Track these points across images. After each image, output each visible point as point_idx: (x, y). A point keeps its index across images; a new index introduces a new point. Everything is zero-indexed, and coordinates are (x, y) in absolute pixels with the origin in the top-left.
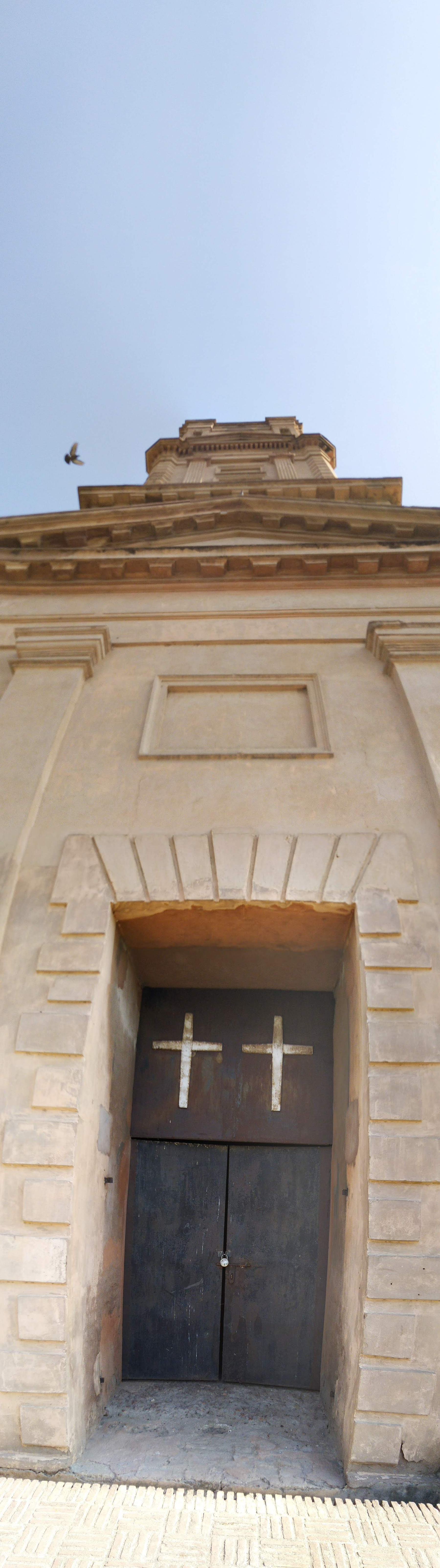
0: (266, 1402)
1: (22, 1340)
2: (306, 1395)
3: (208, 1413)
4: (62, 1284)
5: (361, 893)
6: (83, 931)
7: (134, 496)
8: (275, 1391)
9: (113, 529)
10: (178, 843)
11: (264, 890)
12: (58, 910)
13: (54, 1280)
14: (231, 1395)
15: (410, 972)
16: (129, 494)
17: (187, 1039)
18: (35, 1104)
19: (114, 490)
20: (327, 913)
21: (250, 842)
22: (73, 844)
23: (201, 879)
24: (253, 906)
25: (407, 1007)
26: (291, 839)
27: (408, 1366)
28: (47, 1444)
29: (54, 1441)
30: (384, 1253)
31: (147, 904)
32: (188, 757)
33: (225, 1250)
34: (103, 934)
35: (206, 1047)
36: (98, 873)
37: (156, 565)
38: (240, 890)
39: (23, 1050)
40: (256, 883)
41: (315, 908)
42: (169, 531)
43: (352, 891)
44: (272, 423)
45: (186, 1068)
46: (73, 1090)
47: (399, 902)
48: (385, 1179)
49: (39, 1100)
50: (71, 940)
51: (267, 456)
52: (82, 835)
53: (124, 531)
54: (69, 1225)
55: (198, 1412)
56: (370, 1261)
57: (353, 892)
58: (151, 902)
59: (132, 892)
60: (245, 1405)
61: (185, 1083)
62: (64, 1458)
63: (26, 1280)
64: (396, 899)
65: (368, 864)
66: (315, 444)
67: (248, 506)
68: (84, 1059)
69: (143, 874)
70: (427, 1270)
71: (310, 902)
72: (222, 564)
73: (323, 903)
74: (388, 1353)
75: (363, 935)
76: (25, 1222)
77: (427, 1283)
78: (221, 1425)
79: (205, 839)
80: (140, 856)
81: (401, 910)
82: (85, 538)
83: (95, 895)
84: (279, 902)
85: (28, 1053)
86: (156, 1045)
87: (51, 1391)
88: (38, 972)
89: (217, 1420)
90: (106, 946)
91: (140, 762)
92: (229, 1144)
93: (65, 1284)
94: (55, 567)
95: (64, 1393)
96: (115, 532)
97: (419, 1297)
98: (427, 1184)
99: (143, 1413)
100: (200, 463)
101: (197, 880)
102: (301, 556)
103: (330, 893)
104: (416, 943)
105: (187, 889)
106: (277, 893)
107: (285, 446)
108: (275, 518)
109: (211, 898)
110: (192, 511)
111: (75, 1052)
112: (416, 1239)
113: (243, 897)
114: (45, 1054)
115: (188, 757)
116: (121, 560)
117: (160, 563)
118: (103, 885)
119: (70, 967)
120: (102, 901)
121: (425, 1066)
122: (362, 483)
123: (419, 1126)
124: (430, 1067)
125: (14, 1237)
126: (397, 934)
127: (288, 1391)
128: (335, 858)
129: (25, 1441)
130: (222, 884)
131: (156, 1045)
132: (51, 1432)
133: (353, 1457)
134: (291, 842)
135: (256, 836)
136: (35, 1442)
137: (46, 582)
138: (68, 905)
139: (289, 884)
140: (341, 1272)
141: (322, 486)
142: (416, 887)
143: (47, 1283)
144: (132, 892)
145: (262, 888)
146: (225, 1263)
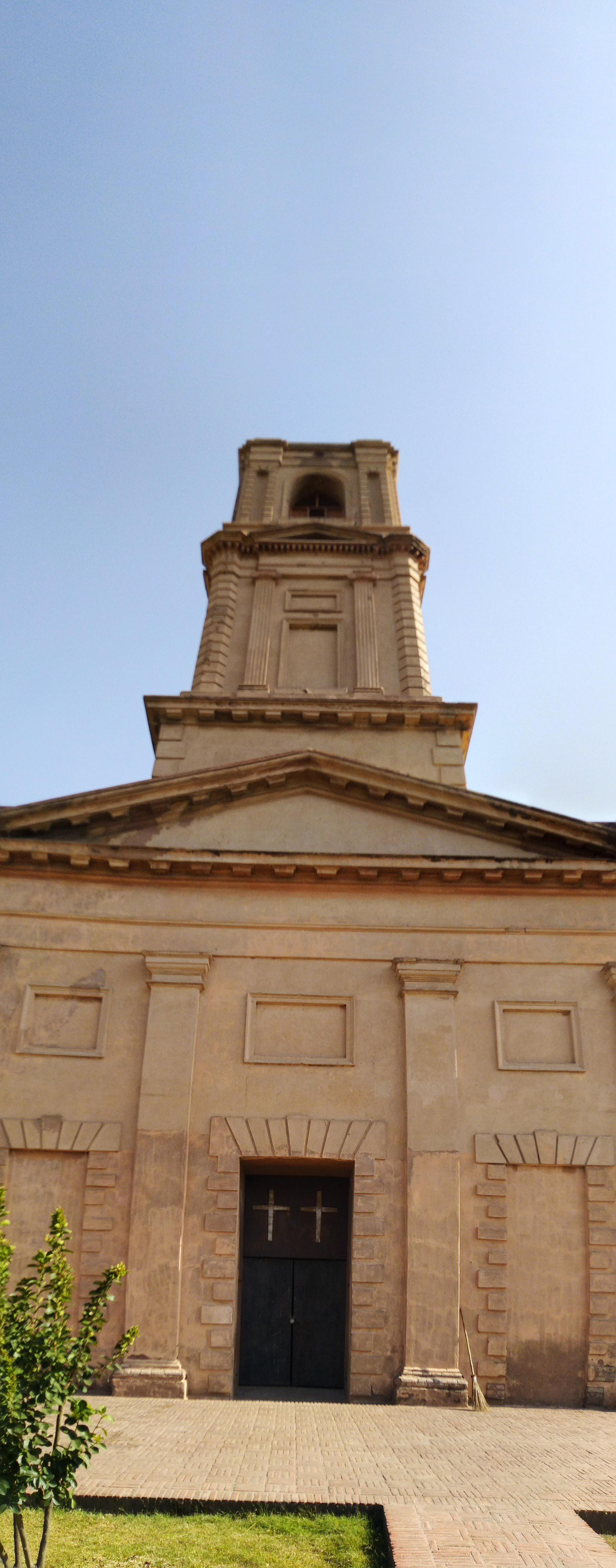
5: (358, 1155)
10: (270, 1124)
11: (313, 1152)
12: (214, 1159)
15: (375, 1196)
16: (197, 710)
17: (271, 1204)
18: (216, 1253)
21: (306, 1124)
22: (216, 1122)
26: (327, 1122)
27: (371, 1354)
33: (292, 1315)
35: (281, 1208)
36: (231, 1141)
45: (271, 1220)
46: (233, 1247)
49: (218, 1251)
50: (222, 1175)
57: (355, 1154)
59: (250, 1152)
61: (270, 1228)
72: (291, 871)
74: (362, 1349)
79: (284, 1122)
80: (252, 1131)
81: (376, 1163)
83: (231, 1153)
85: (211, 1232)
86: (255, 1208)
92: (294, 1259)
98: (376, 1283)
103: (343, 1155)
109: (287, 1156)
110: (265, 771)
114: (219, 1232)
118: (235, 1147)
120: (235, 1155)
126: (373, 1176)
129: (210, 1390)
130: (292, 1148)
131: (255, 1208)
132: (223, 1386)
133: (351, 1393)
144: (250, 1152)
146: (292, 1321)
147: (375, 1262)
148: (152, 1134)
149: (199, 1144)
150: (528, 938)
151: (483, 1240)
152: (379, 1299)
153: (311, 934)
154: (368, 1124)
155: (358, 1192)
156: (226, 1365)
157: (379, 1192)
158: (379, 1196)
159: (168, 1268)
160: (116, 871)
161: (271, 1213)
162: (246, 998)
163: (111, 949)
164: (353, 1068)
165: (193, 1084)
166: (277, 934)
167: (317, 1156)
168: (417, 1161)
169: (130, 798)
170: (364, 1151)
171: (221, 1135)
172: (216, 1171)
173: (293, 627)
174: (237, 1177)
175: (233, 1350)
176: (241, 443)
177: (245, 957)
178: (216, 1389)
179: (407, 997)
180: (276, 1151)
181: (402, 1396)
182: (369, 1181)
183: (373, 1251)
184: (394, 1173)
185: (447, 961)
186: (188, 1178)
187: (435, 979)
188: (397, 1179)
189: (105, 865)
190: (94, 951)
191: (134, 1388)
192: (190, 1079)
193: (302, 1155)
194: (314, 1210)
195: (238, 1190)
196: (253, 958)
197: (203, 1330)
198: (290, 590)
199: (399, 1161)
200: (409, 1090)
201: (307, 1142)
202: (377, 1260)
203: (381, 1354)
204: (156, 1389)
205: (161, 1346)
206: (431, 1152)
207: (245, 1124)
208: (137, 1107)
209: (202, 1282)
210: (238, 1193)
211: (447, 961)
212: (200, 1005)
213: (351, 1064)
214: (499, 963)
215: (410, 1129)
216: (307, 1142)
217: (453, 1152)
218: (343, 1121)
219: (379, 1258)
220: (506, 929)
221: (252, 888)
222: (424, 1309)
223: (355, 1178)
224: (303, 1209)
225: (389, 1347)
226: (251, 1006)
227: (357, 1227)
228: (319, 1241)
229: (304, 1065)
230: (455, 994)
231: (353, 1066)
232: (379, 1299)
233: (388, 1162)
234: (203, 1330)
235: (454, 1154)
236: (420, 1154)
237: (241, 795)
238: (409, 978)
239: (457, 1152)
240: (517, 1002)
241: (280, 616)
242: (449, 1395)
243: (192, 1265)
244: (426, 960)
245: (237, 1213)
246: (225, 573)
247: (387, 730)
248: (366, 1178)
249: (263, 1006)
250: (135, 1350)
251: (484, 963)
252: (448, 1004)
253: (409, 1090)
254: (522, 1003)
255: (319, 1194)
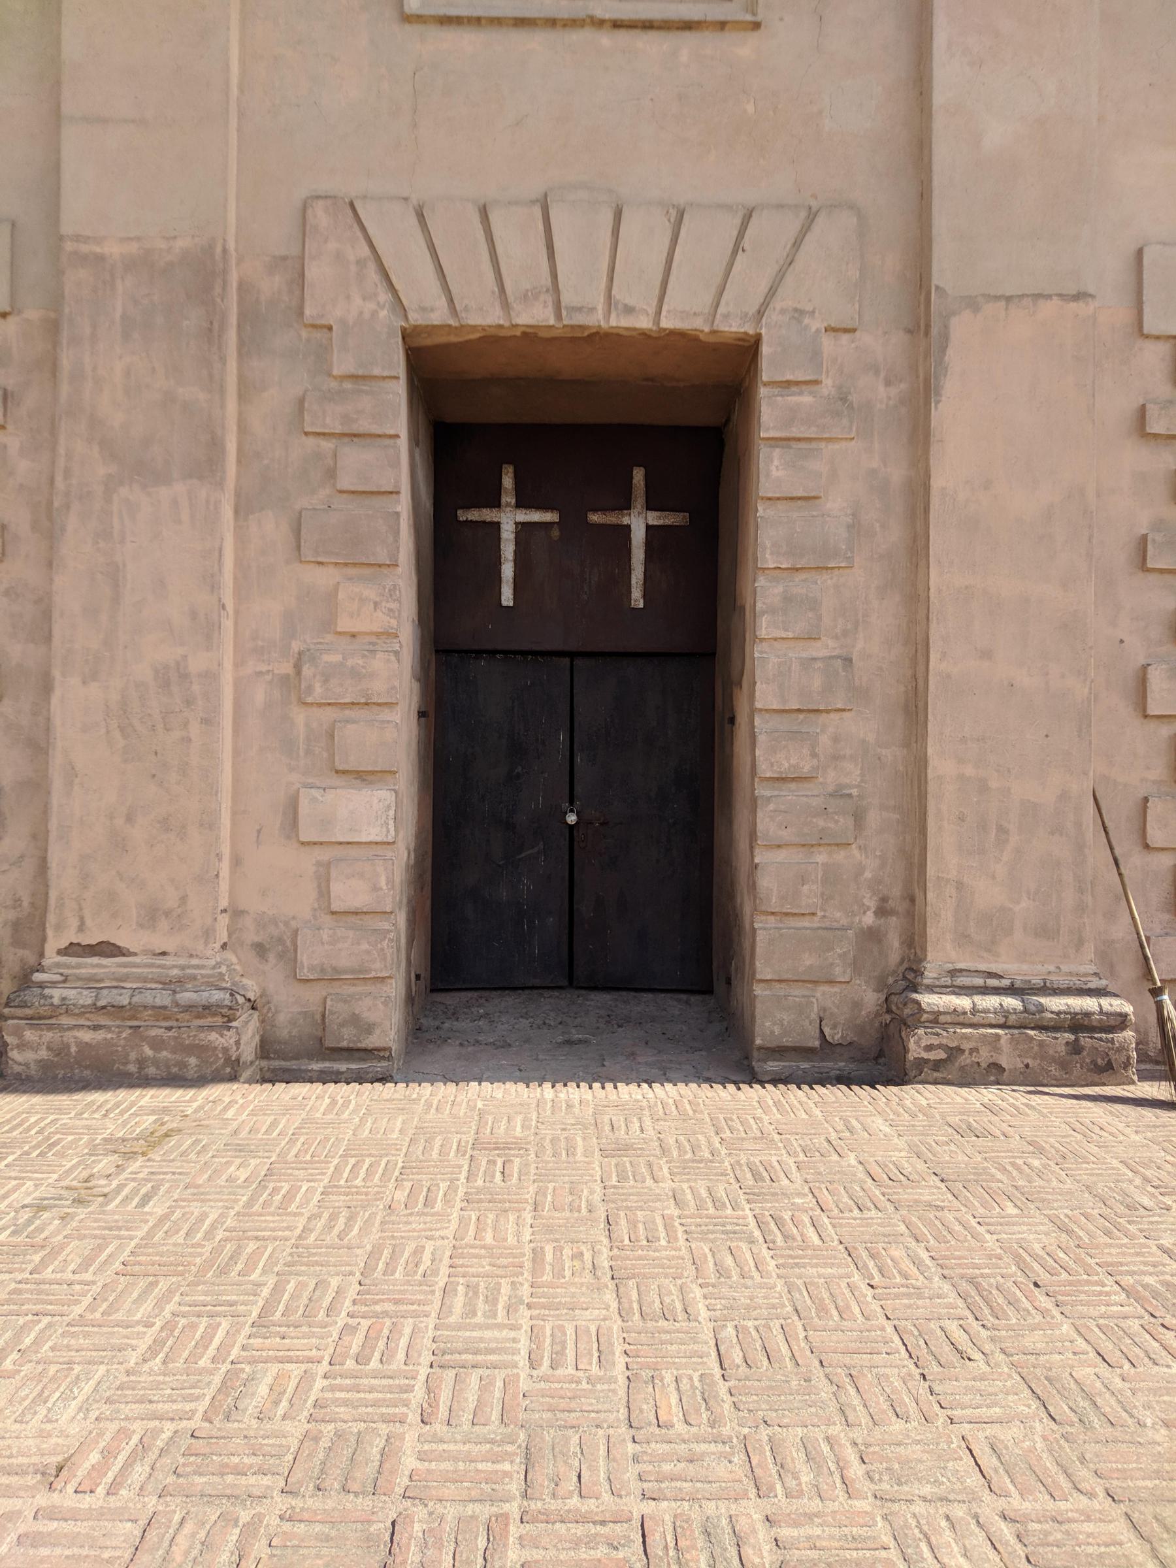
0: (639, 1009)
1: (333, 913)
2: (694, 999)
3: (561, 1023)
4: (388, 843)
5: (772, 316)
6: (366, 373)
8: (650, 996)
10: (495, 217)
11: (629, 310)
12: (318, 335)
13: (379, 839)
14: (588, 1003)
15: (823, 445)
17: (508, 505)
18: (339, 629)
21: (607, 217)
22: (320, 215)
23: (535, 288)
24: (612, 334)
25: (812, 494)
26: (673, 213)
27: (815, 923)
28: (362, 1045)
29: (373, 1041)
30: (776, 793)
32: (497, 22)
33: (571, 802)
35: (536, 516)
36: (373, 275)
38: (592, 310)
39: (313, 560)
40: (618, 297)
41: (702, 337)
45: (508, 550)
46: (391, 610)
48: (774, 707)
50: (348, 385)
52: (335, 197)
54: (395, 773)
55: (547, 1021)
56: (759, 802)
57: (760, 313)
58: (462, 326)
60: (610, 1013)
61: (508, 571)
62: (384, 1064)
63: (341, 840)
68: (400, 570)
70: (830, 810)
71: (696, 330)
73: (714, 332)
74: (787, 908)
76: (337, 772)
77: (831, 825)
78: (580, 1036)
79: (537, 211)
81: (827, 343)
83: (374, 314)
84: (651, 330)
85: (320, 563)
86: (463, 515)
87: (373, 974)
89: (573, 1031)
90: (398, 392)
91: (407, 27)
92: (572, 655)
93: (394, 843)
95: (390, 977)
97: (822, 842)
98: (828, 711)
99: (471, 1024)
101: (527, 291)
103: (726, 316)
105: (515, 306)
106: (648, 315)
109: (552, 322)
111: (388, 562)
112: (814, 775)
113: (599, 321)
114: (346, 564)
115: (497, 22)
118: (384, 296)
120: (387, 320)
121: (829, 571)
123: (819, 644)
124: (836, 572)
125: (324, 789)
126: (816, 382)
127: (669, 995)
129: (329, 1043)
130: (567, 298)
131: (463, 515)
132: (369, 1029)
133: (758, 1042)
134: (672, 220)
136: (344, 1044)
139: (666, 299)
140: (730, 822)
143: (370, 843)
144: (432, 310)
145: (626, 305)
146: (572, 819)
147: (825, 648)
148: (113, 250)
149: (271, 285)
151: (1162, 571)
152: (836, 757)
154: (803, 214)
155: (772, 434)
156: (378, 965)
158: (837, 446)
159: (184, 676)
161: (508, 534)
164: (756, 34)
167: (644, 323)
171: (339, 256)
172: (330, 375)
175: (401, 919)
178: (347, 1037)
180: (517, 306)
181: (925, 1055)
182: (807, 399)
183: (820, 618)
184: (882, 375)
186: (242, 397)
191: (73, 1049)
192: (227, 68)
193: (597, 319)
194: (626, 521)
197: (308, 861)
201: (611, 279)
202: (831, 643)
203: (844, 922)
204: (149, 1052)
205: (167, 914)
206: (1008, 299)
207: (413, 220)
209: (300, 717)
213: (749, 18)
215: (941, 223)
216: (611, 279)
217: (1079, 296)
218: (728, 207)
219: (836, 637)
222: (983, 787)
223: (763, 391)
224: (595, 518)
225: (871, 903)
227: (768, 544)
228: (641, 605)
229: (599, 23)
231: (756, 26)
232: (836, 757)
234: (308, 861)
235: (1081, 304)
236: (972, 304)
242: (1075, 1048)
243: (264, 668)
245: (403, 506)
248: (794, 389)
250: (81, 928)
253: (939, 98)
255: (638, 475)
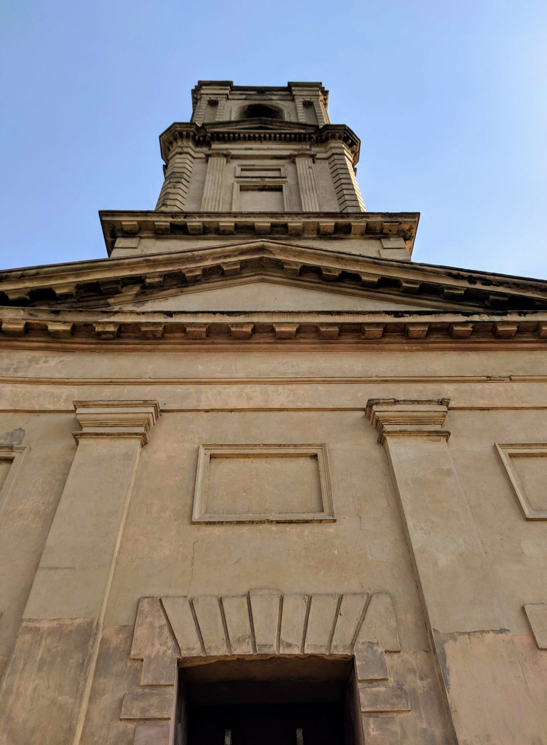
5: (359, 646)
7: (158, 225)
9: (146, 277)
10: (225, 604)
11: (289, 645)
12: (137, 664)
16: (153, 222)
19: (137, 216)
20: (334, 660)
21: (277, 601)
22: (145, 606)
23: (244, 636)
26: (307, 598)
31: (204, 657)
34: (172, 685)
37: (193, 329)
41: (325, 657)
42: (198, 278)
43: (352, 644)
44: (296, 91)
47: (385, 652)
50: (147, 690)
51: (287, 153)
53: (157, 280)
57: (352, 645)
64: (383, 650)
65: (363, 620)
66: (340, 138)
67: (271, 252)
69: (200, 632)
71: (322, 654)
72: (249, 329)
73: (331, 655)
75: (360, 681)
79: (245, 600)
80: (198, 616)
81: (387, 658)
82: (119, 286)
83: (165, 652)
84: (300, 655)
88: (121, 720)
94: (98, 329)
96: (148, 281)
100: (219, 159)
101: (240, 637)
102: (317, 323)
103: (336, 647)
104: (400, 686)
107: (307, 139)
108: (294, 267)
109: (251, 653)
110: (220, 258)
116: (160, 324)
117: (195, 327)
118: (171, 643)
119: (148, 715)
122: (379, 219)
126: (386, 679)
128: (339, 615)
130: (259, 640)
135: (281, 596)
137: (90, 341)
138: (144, 660)
141: (340, 220)
142: (398, 639)
144: (193, 649)
148: (45, 625)
149: (116, 640)
150: (515, 385)
153: (271, 388)
157: (400, 707)
158: (402, 715)
160: (55, 336)
162: (198, 450)
163: (37, 408)
165: (119, 553)
166: (235, 388)
167: (296, 651)
168: (450, 648)
169: (77, 275)
170: (366, 639)
171: (151, 625)
172: (139, 685)
173: (212, 457)
174: (173, 693)
176: (193, 84)
177: (198, 411)
179: (390, 441)
182: (382, 689)
185: (429, 402)
187: (420, 421)
188: (425, 683)
189: (43, 330)
190: (16, 411)
193: (273, 650)
195: (173, 717)
196: (207, 411)
198: (239, 165)
199: (422, 653)
200: (415, 546)
201: (280, 630)
206: (469, 633)
207: (188, 606)
208: (28, 589)
210: (172, 723)
211: (429, 402)
212: (140, 460)
213: (331, 518)
214: (488, 409)
215: (429, 599)
216: (280, 630)
217: (502, 631)
220: (487, 377)
221: (208, 351)
223: (359, 685)
226: (203, 458)
230: (447, 435)
231: (335, 521)
233: (405, 655)
236: (453, 636)
237: (196, 281)
238: (389, 421)
239: (508, 631)
240: (523, 445)
241: (231, 180)
244: (405, 402)
246: (181, 153)
247: (336, 239)
248: (375, 683)
249: (217, 460)
251: (471, 409)
252: (440, 445)
253: (415, 547)
254: (529, 445)
